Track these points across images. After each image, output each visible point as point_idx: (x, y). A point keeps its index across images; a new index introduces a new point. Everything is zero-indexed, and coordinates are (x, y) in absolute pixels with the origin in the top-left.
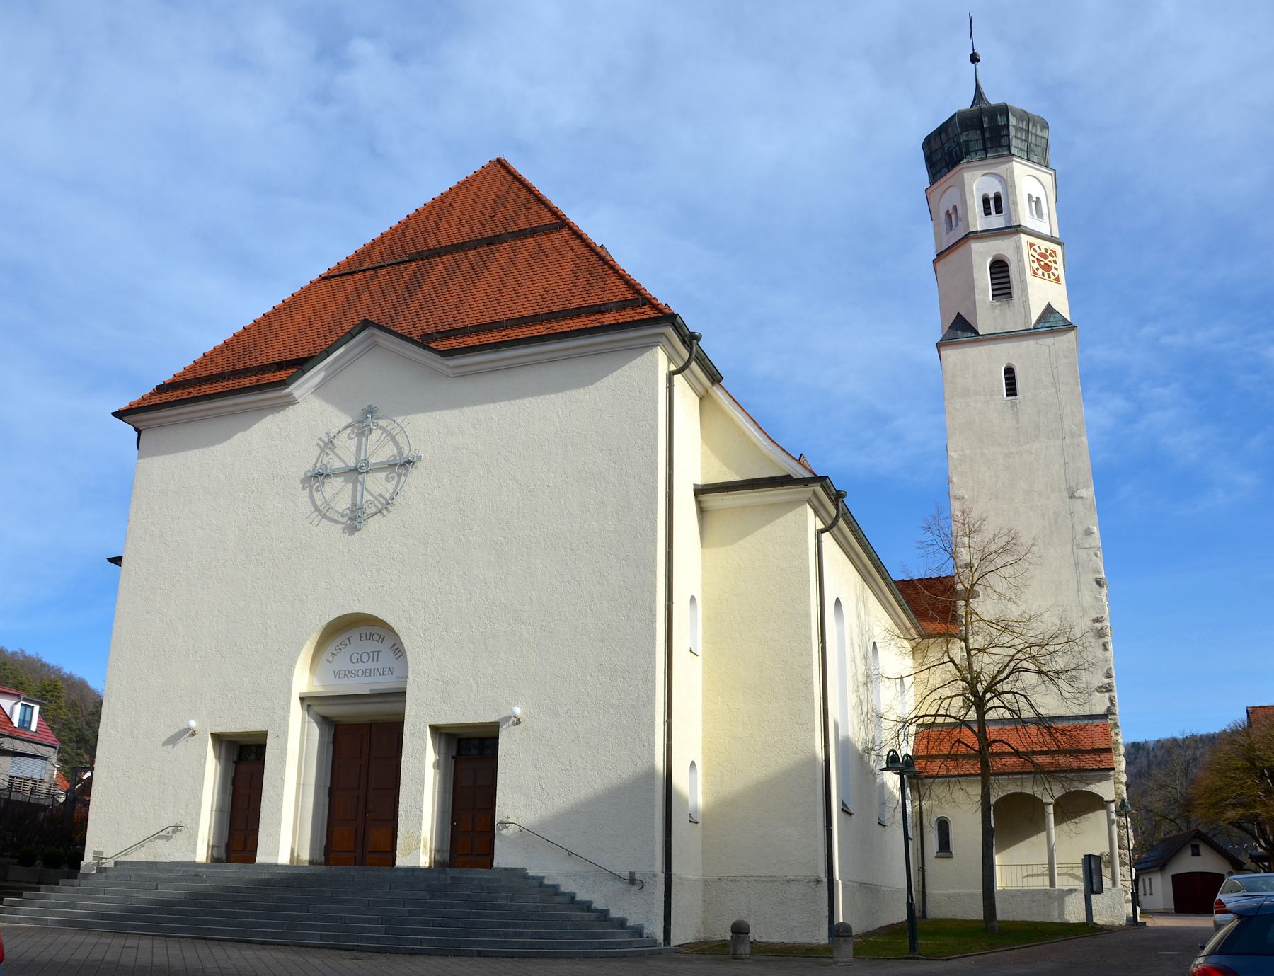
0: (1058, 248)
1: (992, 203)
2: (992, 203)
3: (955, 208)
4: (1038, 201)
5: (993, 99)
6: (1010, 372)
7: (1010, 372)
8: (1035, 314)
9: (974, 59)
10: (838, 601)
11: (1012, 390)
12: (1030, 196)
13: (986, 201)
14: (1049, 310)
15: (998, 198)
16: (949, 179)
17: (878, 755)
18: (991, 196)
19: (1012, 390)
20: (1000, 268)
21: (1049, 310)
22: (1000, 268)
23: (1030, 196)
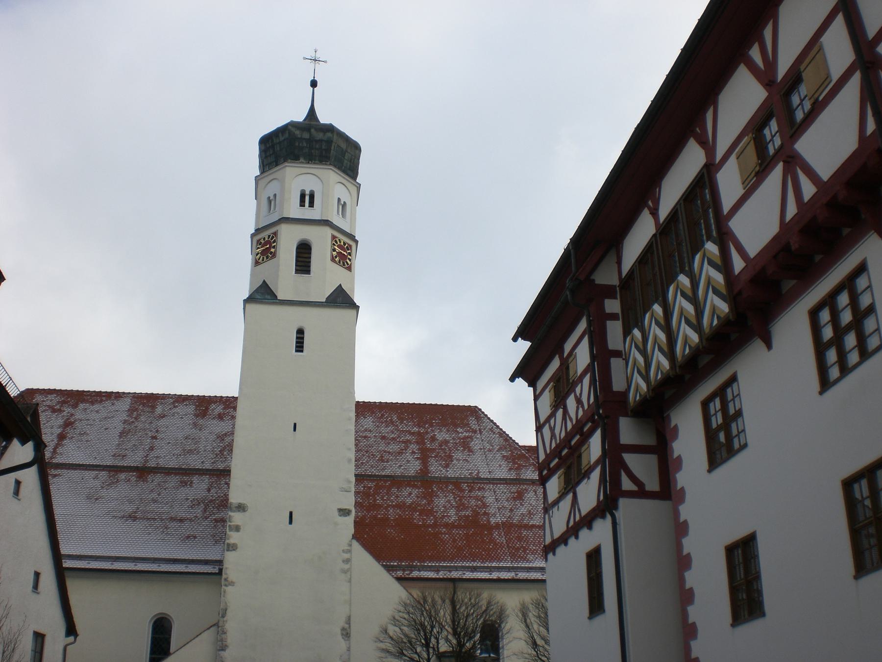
9: (314, 84)
11: (300, 347)
12: (339, 200)
13: (303, 196)
15: (312, 196)
18: (307, 192)
19: (300, 347)
20: (304, 251)
22: (304, 251)
23: (339, 200)
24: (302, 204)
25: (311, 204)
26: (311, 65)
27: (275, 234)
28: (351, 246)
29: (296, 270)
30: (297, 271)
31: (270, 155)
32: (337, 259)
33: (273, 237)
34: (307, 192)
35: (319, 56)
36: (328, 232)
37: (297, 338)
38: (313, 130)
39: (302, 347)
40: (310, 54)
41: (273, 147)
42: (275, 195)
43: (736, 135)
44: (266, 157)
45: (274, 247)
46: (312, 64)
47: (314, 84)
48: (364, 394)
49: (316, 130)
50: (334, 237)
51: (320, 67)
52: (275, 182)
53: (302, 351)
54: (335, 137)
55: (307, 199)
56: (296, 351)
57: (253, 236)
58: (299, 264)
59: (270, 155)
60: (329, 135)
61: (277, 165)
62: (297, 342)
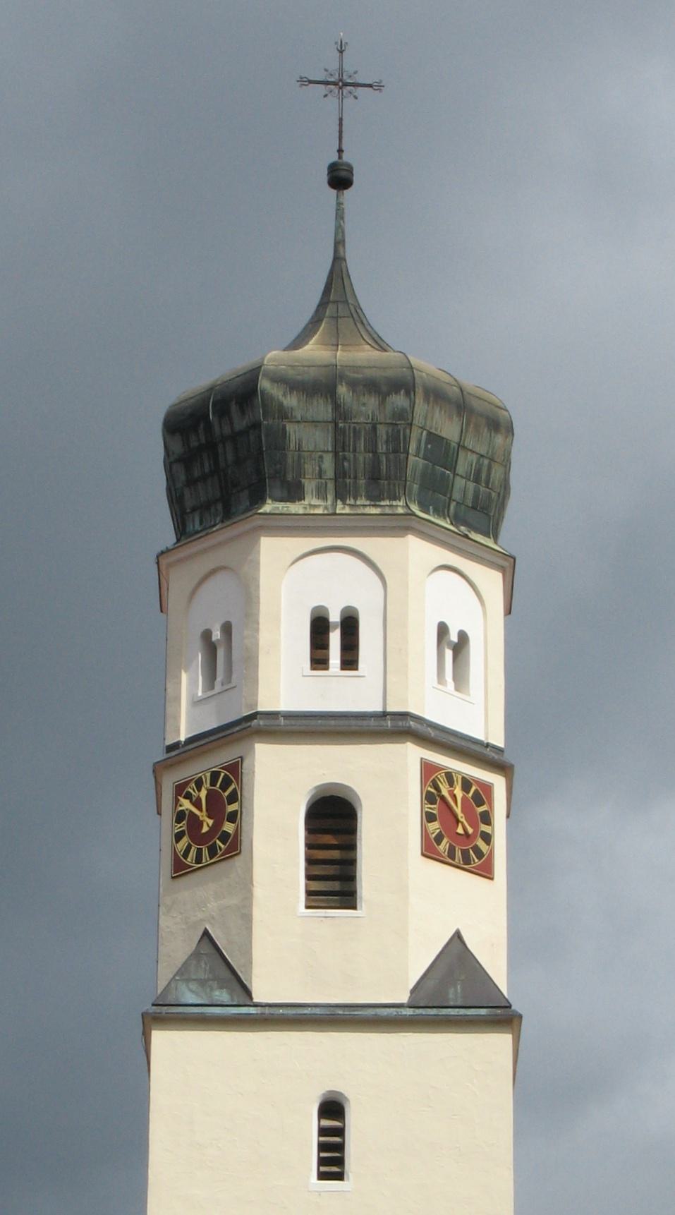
0: (498, 783)
1: (335, 638)
2: (335, 638)
3: (227, 629)
4: (461, 646)
5: (334, 192)
6: (332, 1108)
7: (332, 1108)
8: (418, 960)
9: (340, 179)
10: (159, 813)
11: (332, 1161)
12: (443, 630)
13: (319, 626)
14: (456, 955)
15: (350, 625)
16: (216, 546)
17: (321, 474)
18: (335, 617)
19: (332, 1161)
20: (332, 819)
21: (456, 955)
22: (332, 819)
23: (443, 630)
24: (319, 661)
25: (350, 661)
26: (324, 105)
27: (235, 770)
28: (488, 788)
29: (309, 893)
30: (315, 898)
31: (204, 478)
32: (443, 846)
33: (226, 783)
34: (335, 617)
35: (359, 66)
36: (412, 755)
37: (323, 1132)
38: (342, 390)
39: (340, 1162)
40: (324, 63)
41: (211, 447)
42: (227, 629)
43: (321, 287)
44: (191, 482)
45: (233, 817)
46: (333, 102)
47: (340, 179)
48: (501, 1042)
49: (353, 385)
50: (428, 770)
51: (360, 105)
52: (220, 578)
53: (339, 1176)
54: (421, 407)
55: (335, 638)
56: (322, 1176)
57: (159, 769)
58: (318, 870)
59: (204, 478)
60: (399, 400)
61: (228, 514)
62: (322, 1147)
